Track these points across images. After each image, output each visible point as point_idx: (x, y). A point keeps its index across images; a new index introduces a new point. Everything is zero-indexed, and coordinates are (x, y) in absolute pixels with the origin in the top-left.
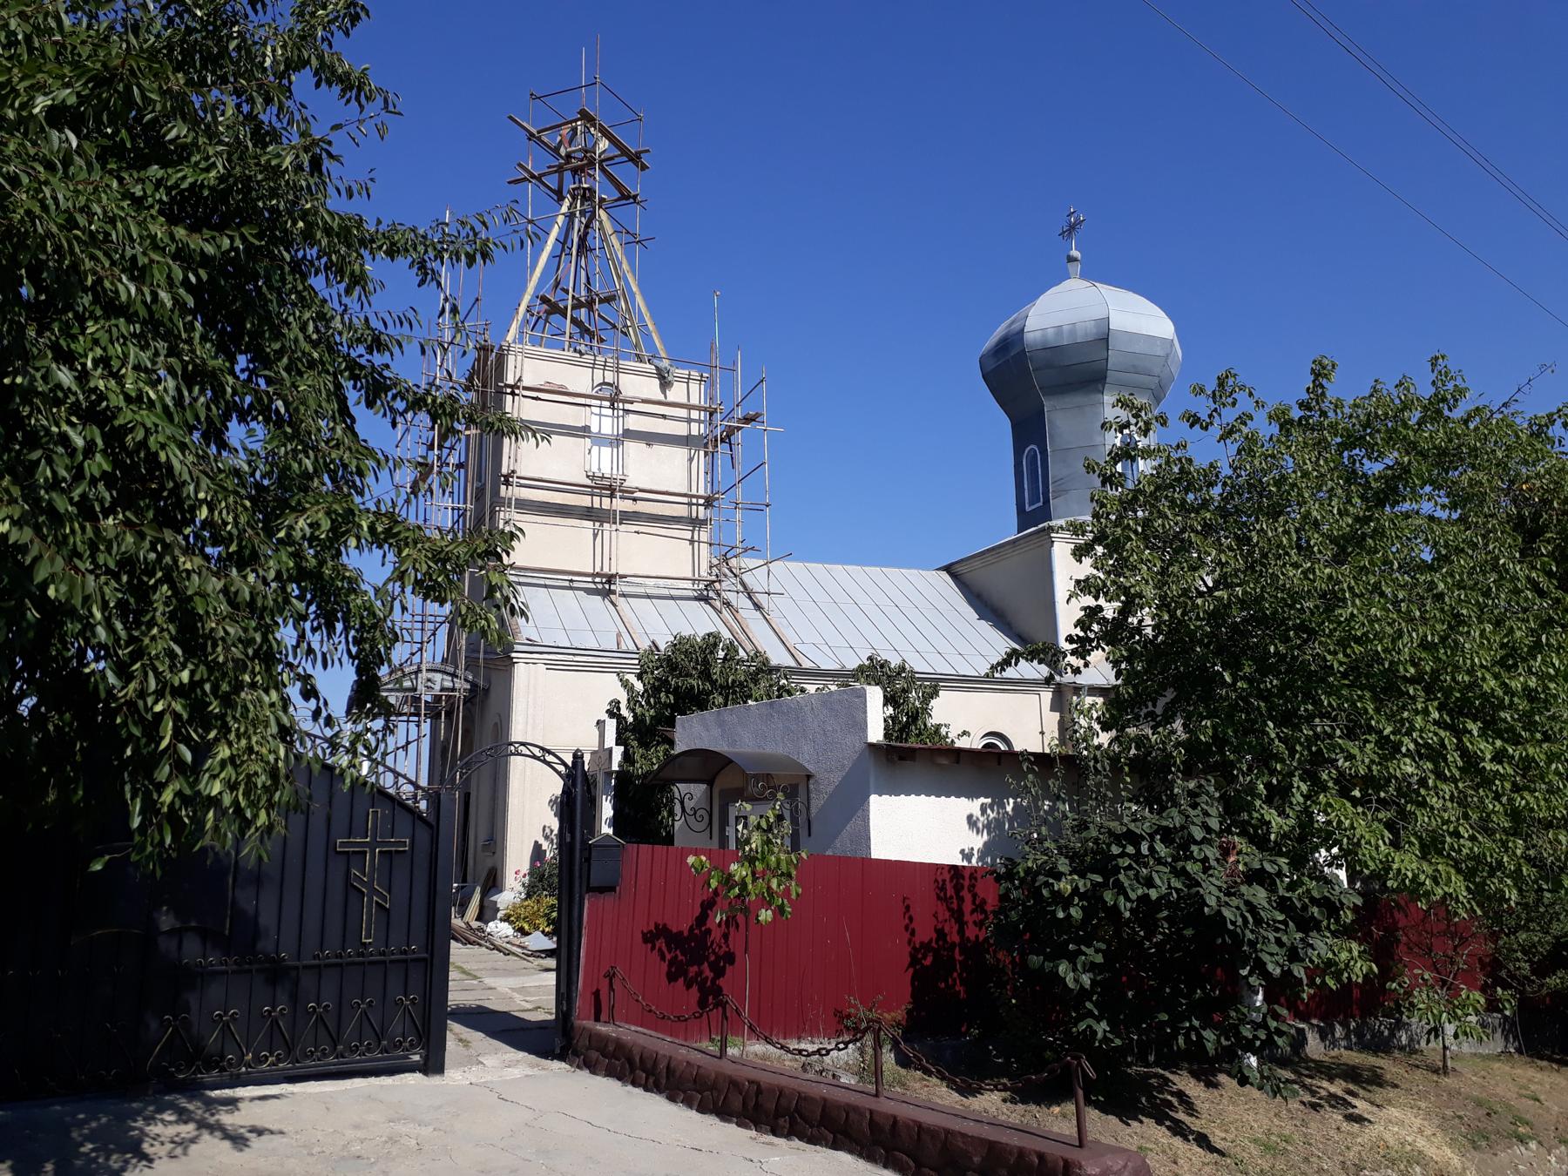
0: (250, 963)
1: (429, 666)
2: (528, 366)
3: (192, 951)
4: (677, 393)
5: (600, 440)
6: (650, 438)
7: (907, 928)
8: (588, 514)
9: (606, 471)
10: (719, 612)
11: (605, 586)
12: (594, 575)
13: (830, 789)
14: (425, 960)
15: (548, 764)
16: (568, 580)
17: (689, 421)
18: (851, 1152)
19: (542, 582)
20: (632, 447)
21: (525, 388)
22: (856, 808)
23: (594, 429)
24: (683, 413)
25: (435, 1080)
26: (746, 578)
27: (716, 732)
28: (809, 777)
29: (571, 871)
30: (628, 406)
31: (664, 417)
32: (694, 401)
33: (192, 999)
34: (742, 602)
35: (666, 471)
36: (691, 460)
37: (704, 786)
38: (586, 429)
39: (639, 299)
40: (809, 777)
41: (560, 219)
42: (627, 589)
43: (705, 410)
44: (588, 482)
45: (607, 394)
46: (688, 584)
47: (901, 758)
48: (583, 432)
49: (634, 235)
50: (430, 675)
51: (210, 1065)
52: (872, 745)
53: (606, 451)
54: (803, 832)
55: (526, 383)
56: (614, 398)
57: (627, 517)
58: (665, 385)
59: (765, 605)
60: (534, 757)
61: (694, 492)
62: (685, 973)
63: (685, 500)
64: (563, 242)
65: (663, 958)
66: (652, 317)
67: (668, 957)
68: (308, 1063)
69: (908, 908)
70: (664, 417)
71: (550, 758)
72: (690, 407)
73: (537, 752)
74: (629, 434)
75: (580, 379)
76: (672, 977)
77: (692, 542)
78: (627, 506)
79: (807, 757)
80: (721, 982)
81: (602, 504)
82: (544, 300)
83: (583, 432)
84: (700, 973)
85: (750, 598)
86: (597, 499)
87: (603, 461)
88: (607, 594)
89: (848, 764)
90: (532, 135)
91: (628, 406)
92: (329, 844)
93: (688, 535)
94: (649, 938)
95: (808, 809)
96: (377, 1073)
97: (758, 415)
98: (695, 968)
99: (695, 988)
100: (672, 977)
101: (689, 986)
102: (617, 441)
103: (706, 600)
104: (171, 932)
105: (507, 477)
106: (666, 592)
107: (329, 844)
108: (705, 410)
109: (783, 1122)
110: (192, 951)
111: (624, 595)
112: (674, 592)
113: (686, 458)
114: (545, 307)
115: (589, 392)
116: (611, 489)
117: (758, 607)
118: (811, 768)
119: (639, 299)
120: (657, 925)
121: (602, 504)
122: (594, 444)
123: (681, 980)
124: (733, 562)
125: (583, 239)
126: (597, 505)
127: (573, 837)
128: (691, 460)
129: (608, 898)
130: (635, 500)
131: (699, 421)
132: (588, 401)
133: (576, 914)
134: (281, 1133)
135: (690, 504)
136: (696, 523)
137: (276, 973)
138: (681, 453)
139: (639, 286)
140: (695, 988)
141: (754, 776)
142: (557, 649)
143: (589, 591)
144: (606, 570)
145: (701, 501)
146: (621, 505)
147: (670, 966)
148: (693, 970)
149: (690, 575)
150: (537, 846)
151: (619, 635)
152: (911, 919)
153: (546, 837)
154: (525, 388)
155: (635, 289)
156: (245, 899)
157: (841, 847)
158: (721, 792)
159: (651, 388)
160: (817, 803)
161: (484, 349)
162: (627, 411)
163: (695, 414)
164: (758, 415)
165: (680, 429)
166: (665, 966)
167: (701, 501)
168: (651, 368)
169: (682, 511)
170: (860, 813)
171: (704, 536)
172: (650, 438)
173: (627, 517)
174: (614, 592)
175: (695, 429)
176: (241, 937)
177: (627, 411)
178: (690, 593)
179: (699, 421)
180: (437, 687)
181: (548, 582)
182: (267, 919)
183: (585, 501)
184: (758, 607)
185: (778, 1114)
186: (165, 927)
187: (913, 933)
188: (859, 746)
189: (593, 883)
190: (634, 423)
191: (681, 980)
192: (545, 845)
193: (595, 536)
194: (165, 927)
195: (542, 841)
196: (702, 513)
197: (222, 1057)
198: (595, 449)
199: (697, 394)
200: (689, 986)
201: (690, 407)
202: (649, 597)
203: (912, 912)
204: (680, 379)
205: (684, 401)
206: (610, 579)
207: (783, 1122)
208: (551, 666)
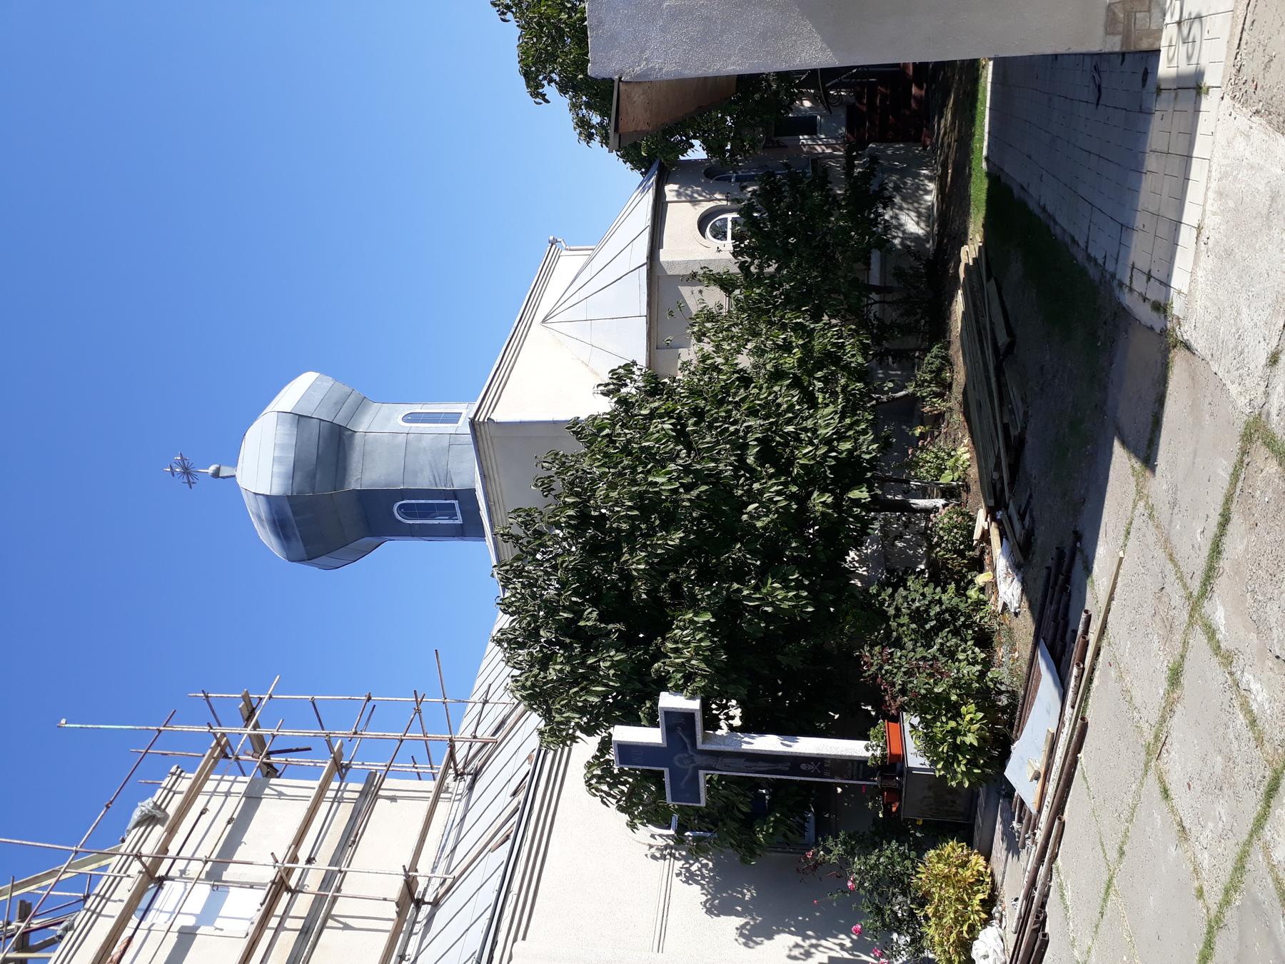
153: (808, 955)
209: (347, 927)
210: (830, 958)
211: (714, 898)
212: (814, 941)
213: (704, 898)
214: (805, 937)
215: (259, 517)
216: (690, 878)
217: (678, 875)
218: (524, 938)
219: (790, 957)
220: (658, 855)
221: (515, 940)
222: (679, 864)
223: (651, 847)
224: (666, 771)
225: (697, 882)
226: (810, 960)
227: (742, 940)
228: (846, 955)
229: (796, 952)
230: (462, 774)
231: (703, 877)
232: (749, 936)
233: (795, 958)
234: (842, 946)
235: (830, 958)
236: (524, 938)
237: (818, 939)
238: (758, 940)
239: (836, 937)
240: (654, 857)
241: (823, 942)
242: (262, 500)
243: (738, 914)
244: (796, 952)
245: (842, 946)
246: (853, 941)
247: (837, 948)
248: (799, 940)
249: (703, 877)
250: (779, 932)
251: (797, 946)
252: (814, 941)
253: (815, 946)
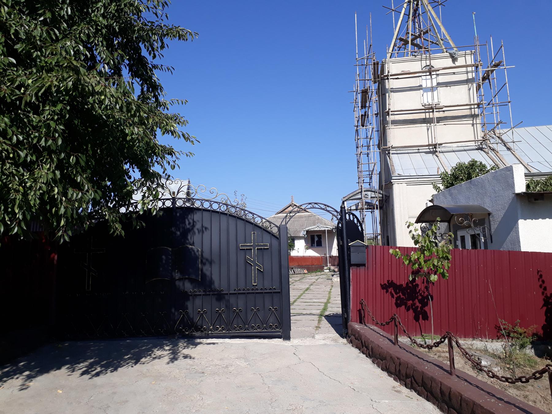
0: (209, 292)
1: (365, 189)
2: (393, 67)
3: (188, 286)
4: (461, 61)
5: (426, 90)
6: (447, 84)
7: (541, 286)
8: (424, 121)
9: (430, 102)
10: (487, 153)
11: (433, 149)
12: (429, 145)
13: (500, 219)
14: (279, 292)
15: (328, 211)
16: (417, 149)
17: (467, 72)
18: (434, 404)
19: (406, 151)
20: (441, 90)
21: (391, 75)
22: (510, 225)
23: (424, 86)
24: (464, 69)
25: (288, 342)
26: (503, 137)
27: (449, 198)
28: (489, 214)
29: (343, 257)
30: (438, 73)
31: (454, 73)
32: (469, 63)
33: (189, 304)
34: (500, 148)
35: (460, 96)
36: (469, 89)
37: (446, 224)
38: (421, 86)
39: (443, 29)
40: (489, 214)
41: (405, 5)
42: (443, 149)
43: (473, 66)
44: (423, 108)
45: (427, 70)
46: (473, 143)
47: (536, 200)
48: (419, 88)
49: (438, 2)
50: (366, 193)
51: (198, 329)
52: (518, 195)
53: (430, 94)
54: (489, 241)
56: (430, 71)
57: (439, 120)
58: (454, 59)
59: (512, 148)
60: (322, 209)
61: (472, 102)
62: (406, 304)
63: (468, 107)
64: (407, 15)
65: (393, 296)
66: (449, 33)
67: (395, 296)
68: (234, 331)
69: (541, 276)
70: (454, 73)
71: (329, 209)
72: (466, 66)
73: (323, 207)
74: (439, 84)
75: (416, 66)
76: (398, 305)
77: (473, 125)
78: (441, 115)
79: (488, 206)
80: (426, 309)
81: (429, 116)
82: (401, 40)
83: (419, 88)
84: (413, 304)
85: (505, 146)
86: (427, 114)
87: (428, 98)
88: (434, 153)
89: (507, 206)
91: (438, 73)
92: (237, 247)
93: (471, 122)
94: (384, 287)
95: (490, 230)
96: (265, 337)
97: (500, 62)
98: (411, 302)
99: (411, 311)
100: (398, 305)
101: (408, 310)
102: (432, 89)
103: (481, 149)
104: (180, 279)
106: (462, 148)
107: (237, 247)
108: (473, 66)
109: (408, 381)
110: (188, 286)
111: (440, 152)
112: (466, 148)
113: (467, 89)
114: (402, 42)
115: (420, 70)
116: (431, 108)
117: (509, 149)
118: (490, 210)
119: (443, 29)
120: (388, 281)
121: (429, 116)
122: (424, 92)
123: (403, 307)
124: (497, 131)
125: (416, 11)
126: (428, 117)
127: (343, 242)
129: (362, 268)
130: (444, 111)
131: (472, 72)
132: (420, 74)
133: (347, 276)
134: (191, 358)
135: (471, 109)
136: (474, 116)
137: (220, 296)
138: (465, 87)
139: (443, 23)
140: (411, 311)
141: (457, 215)
142: (411, 177)
143: (426, 153)
144: (434, 143)
146: (437, 115)
147: (396, 300)
148: (410, 303)
149: (473, 139)
151: (438, 168)
152: (543, 282)
154: (391, 75)
155: (440, 24)
156: (206, 269)
157: (506, 247)
158: (453, 225)
159: (449, 62)
160: (494, 227)
161: (376, 64)
162: (438, 75)
163: (470, 69)
164: (500, 62)
165: (464, 77)
166: (394, 300)
167: (476, 106)
168: (448, 54)
169: (467, 112)
170: (514, 229)
171: (479, 121)
172: (447, 84)
173: (439, 120)
174: (437, 152)
175: (470, 76)
176: (204, 283)
177: (438, 75)
178: (474, 148)
179: (472, 72)
180: (369, 197)
181: (409, 151)
182: (215, 278)
183: (423, 116)
184: (509, 149)
185: (407, 376)
186: (177, 278)
187: (545, 289)
188: (512, 196)
189: (352, 263)
190: (441, 79)
191: (403, 307)
193: (428, 129)
194: (177, 278)
196: (477, 111)
197: (202, 327)
198: (425, 94)
199: (470, 60)
200: (408, 310)
201: (466, 66)
202: (454, 151)
203: (543, 278)
204: (461, 56)
205: (464, 64)
206: (435, 146)
207: (408, 381)
208: (408, 184)
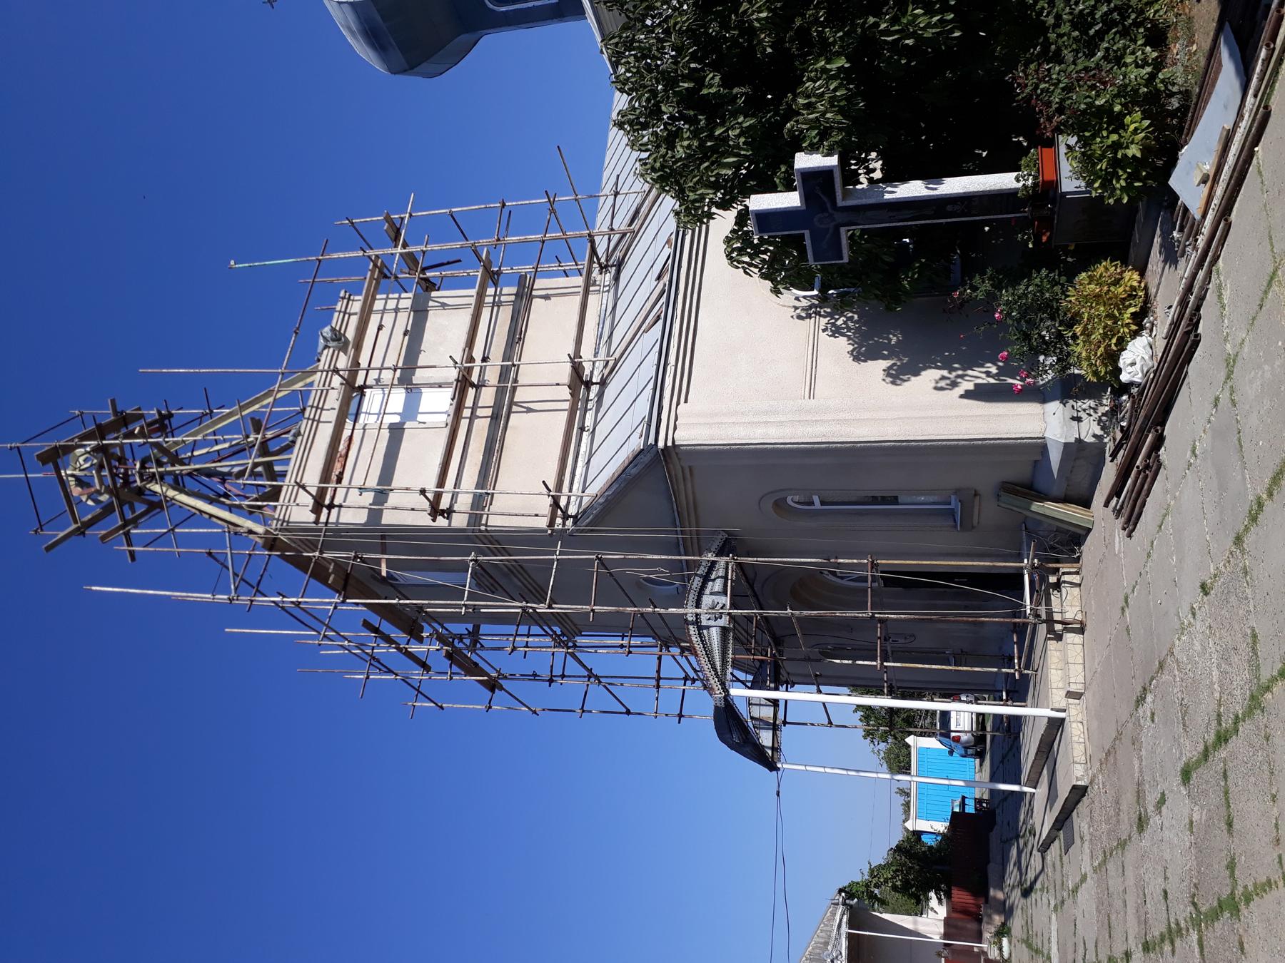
8: (499, 419)
21: (441, 482)
23: (397, 419)
36: (444, 305)
46: (593, 300)
55: (431, 486)
81: (485, 398)
90: (78, 529)
105: (435, 511)
122: (414, 419)
128: (444, 305)
145: (490, 291)
150: (967, 395)
153: (954, 384)
154: (441, 482)
165: (505, 314)
170: (464, 38)
192: (968, 385)
195: (960, 390)
198: (420, 418)
209: (530, 410)
210: (976, 385)
211: (860, 346)
212: (960, 372)
213: (851, 348)
214: (951, 370)
215: (350, 29)
216: (836, 332)
217: (824, 331)
218: (686, 401)
219: (936, 388)
220: (803, 314)
221: (678, 404)
222: (824, 321)
223: (796, 308)
224: (807, 233)
225: (843, 335)
226: (957, 389)
227: (889, 379)
228: (992, 381)
229: (942, 384)
230: (606, 266)
231: (849, 329)
232: (895, 376)
233: (942, 389)
234: (988, 374)
235: (976, 385)
236: (686, 401)
237: (965, 370)
238: (905, 377)
239: (982, 366)
240: (799, 317)
241: (970, 372)
242: (347, 8)
243: (885, 358)
244: (942, 384)
245: (988, 374)
246: (999, 368)
247: (983, 376)
248: (945, 373)
249: (849, 329)
250: (925, 369)
251: (943, 378)
252: (960, 372)
253: (961, 377)
